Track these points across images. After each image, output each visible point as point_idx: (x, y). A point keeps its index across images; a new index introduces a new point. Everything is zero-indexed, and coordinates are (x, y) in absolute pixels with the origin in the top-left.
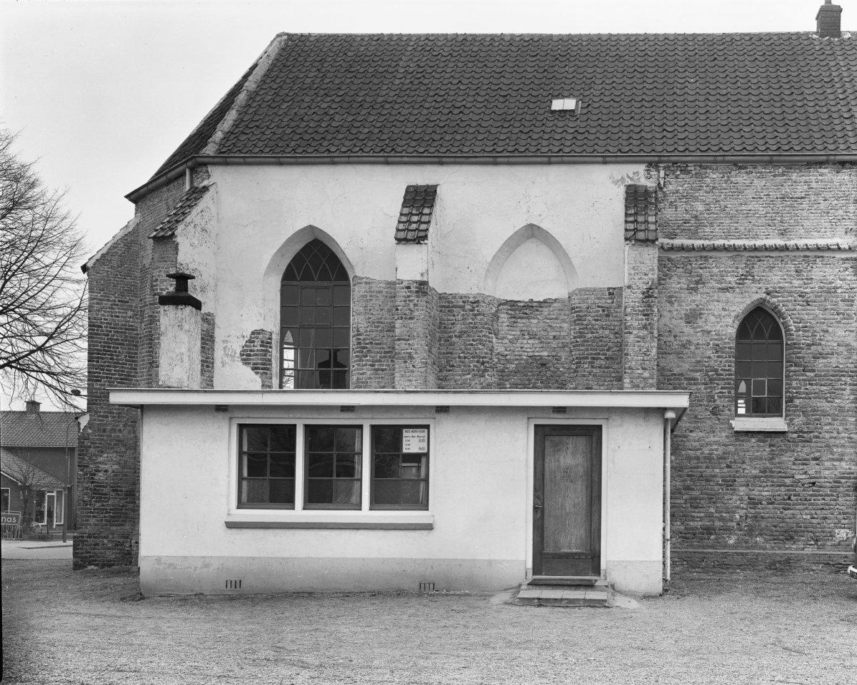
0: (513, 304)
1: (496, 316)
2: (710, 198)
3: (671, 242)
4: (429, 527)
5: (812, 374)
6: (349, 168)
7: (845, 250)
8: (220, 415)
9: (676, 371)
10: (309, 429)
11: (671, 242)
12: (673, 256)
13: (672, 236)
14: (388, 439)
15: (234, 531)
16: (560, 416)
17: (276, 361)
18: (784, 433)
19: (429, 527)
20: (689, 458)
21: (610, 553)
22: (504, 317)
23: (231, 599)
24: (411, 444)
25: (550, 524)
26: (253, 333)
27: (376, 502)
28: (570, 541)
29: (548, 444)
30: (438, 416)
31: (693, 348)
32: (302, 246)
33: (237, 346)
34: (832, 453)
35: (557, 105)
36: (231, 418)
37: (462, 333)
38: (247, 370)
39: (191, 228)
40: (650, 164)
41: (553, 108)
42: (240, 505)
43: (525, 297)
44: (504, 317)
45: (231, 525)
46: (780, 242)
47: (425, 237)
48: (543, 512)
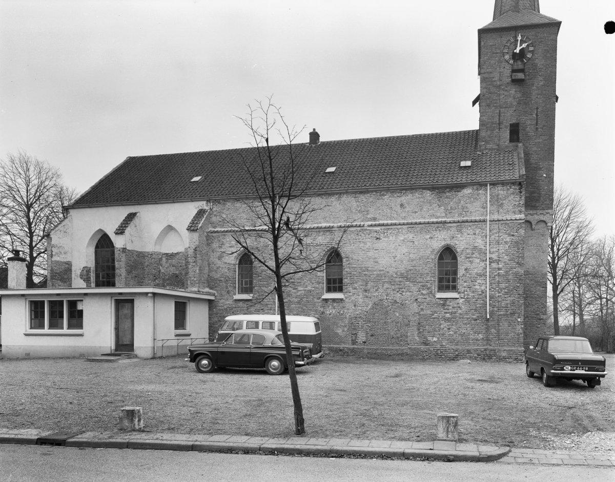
0: (167, 254)
1: (161, 259)
2: (228, 212)
3: (213, 229)
4: (81, 335)
5: (261, 278)
6: (112, 208)
7: (518, 220)
8: (23, 298)
9: (215, 277)
10: (50, 302)
11: (213, 229)
12: (214, 235)
13: (215, 227)
14: (73, 304)
15: (27, 337)
16: (57, 297)
17: (93, 277)
18: (251, 300)
19: (81, 335)
20: (220, 310)
21: (137, 344)
22: (164, 259)
23: (26, 359)
24: (80, 307)
25: (121, 334)
26: (83, 268)
27: (70, 327)
28: (126, 341)
29: (120, 306)
30: (84, 296)
31: (221, 269)
32: (100, 236)
33: (79, 272)
34: (268, 307)
35: (463, 164)
36: (112, 297)
37: (148, 265)
38: (82, 281)
39: (59, 232)
40: (207, 201)
41: (461, 166)
42: (31, 328)
43: (170, 252)
44: (164, 259)
45: (26, 335)
46: (254, 228)
47: (124, 232)
48: (118, 330)
